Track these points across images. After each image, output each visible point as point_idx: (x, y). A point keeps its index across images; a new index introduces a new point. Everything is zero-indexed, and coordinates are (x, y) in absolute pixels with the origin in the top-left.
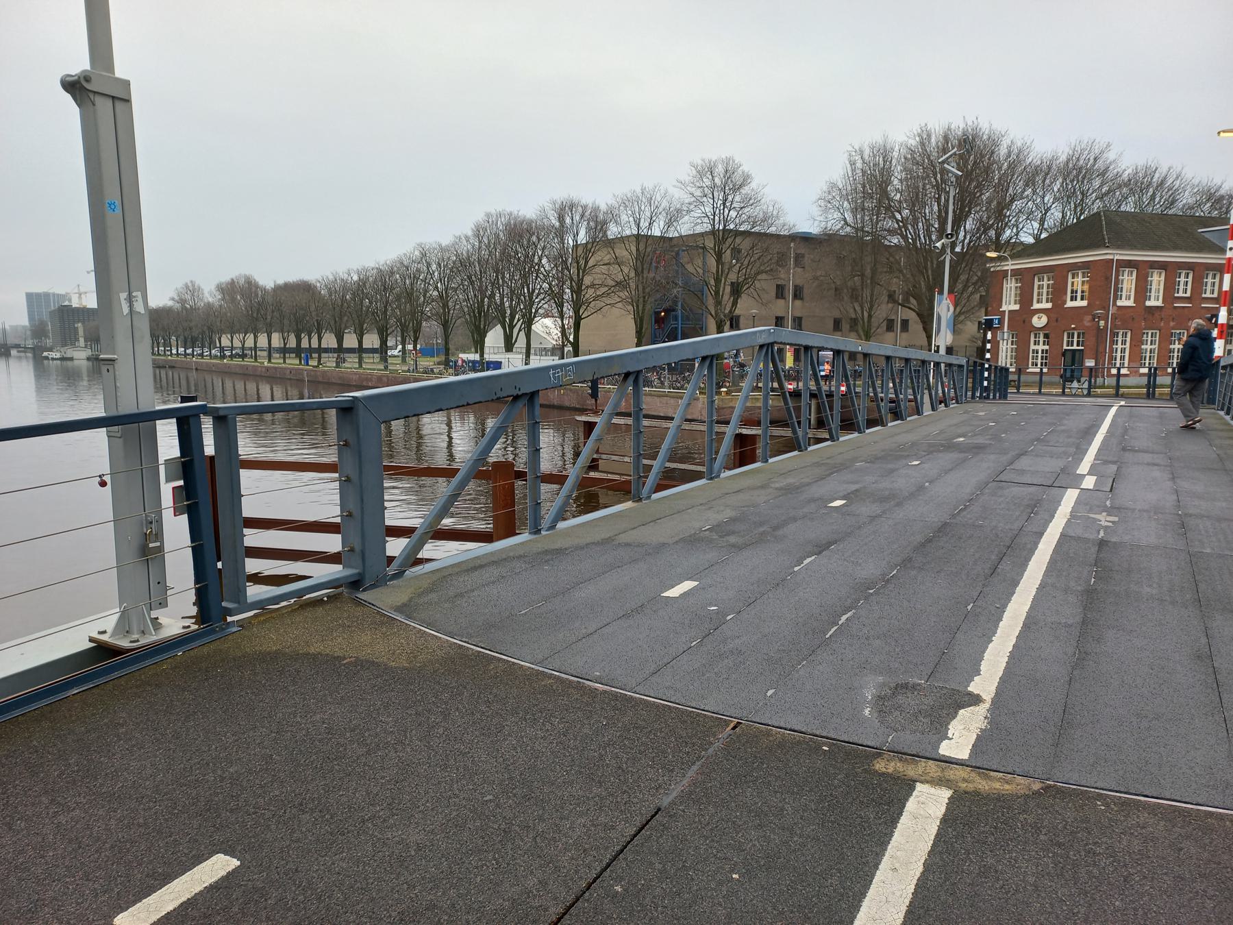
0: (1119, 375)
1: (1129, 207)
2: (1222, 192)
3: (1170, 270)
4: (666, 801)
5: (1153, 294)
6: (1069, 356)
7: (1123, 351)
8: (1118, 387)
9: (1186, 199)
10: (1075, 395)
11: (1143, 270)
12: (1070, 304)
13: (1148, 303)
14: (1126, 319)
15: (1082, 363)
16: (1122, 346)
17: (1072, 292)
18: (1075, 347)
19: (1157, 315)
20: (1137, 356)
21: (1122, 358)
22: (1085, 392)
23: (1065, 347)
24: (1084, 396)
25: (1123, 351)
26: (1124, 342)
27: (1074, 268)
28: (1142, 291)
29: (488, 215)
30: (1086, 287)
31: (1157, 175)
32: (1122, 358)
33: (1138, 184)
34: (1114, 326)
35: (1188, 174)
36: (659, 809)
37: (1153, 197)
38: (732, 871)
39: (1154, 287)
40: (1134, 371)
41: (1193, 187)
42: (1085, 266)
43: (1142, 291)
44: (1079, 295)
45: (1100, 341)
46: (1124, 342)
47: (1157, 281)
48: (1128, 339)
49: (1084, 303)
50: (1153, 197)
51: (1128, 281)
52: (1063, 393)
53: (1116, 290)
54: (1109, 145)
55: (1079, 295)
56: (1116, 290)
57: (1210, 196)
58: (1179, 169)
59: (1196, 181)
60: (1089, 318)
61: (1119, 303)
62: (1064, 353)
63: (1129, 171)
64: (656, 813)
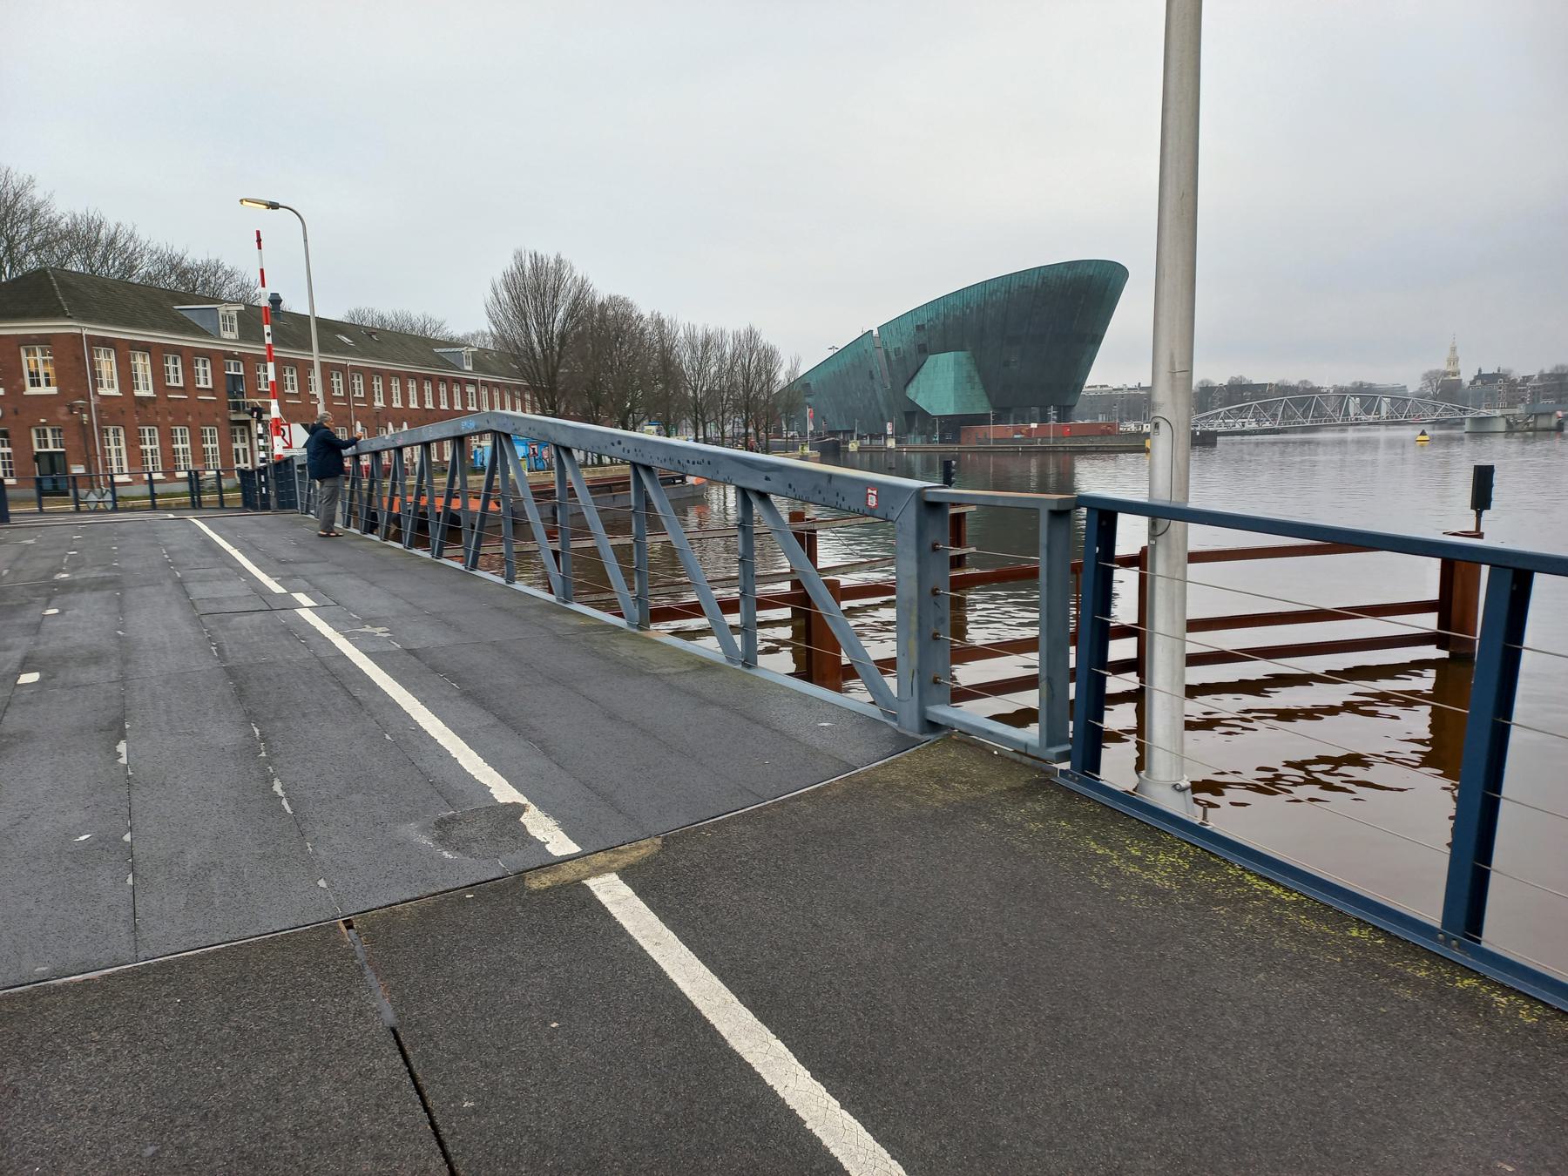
0: (151, 482)
1: (76, 265)
2: (185, 264)
3: (157, 353)
4: (389, 1017)
5: (141, 382)
6: (45, 461)
7: (119, 452)
8: (153, 496)
9: (144, 267)
10: (95, 511)
11: (125, 351)
12: (31, 391)
13: (137, 393)
14: (113, 412)
15: (67, 470)
16: (116, 447)
17: (31, 374)
18: (51, 449)
19: (150, 406)
20: (137, 458)
21: (120, 462)
22: (110, 506)
23: (37, 449)
24: (106, 511)
25: (119, 452)
26: (118, 442)
27: (29, 341)
28: (127, 377)
29: (752, 335)
30: (50, 369)
31: (103, 232)
32: (120, 462)
33: (83, 238)
34: (101, 422)
35: (143, 235)
36: (394, 1030)
37: (105, 258)
38: (546, 1024)
39: (140, 372)
40: (170, 472)
41: (152, 253)
42: (44, 340)
43: (127, 377)
44: (42, 379)
45: (85, 440)
46: (118, 442)
47: (142, 365)
48: (122, 438)
49: (53, 390)
50: (105, 258)
51: (107, 365)
52: (78, 510)
53: (94, 374)
54: (31, 180)
55: (42, 379)
56: (94, 374)
57: (173, 268)
58: (130, 228)
59: (153, 246)
60: (64, 410)
61: (101, 392)
62: (38, 457)
63: (66, 219)
64: (397, 1037)
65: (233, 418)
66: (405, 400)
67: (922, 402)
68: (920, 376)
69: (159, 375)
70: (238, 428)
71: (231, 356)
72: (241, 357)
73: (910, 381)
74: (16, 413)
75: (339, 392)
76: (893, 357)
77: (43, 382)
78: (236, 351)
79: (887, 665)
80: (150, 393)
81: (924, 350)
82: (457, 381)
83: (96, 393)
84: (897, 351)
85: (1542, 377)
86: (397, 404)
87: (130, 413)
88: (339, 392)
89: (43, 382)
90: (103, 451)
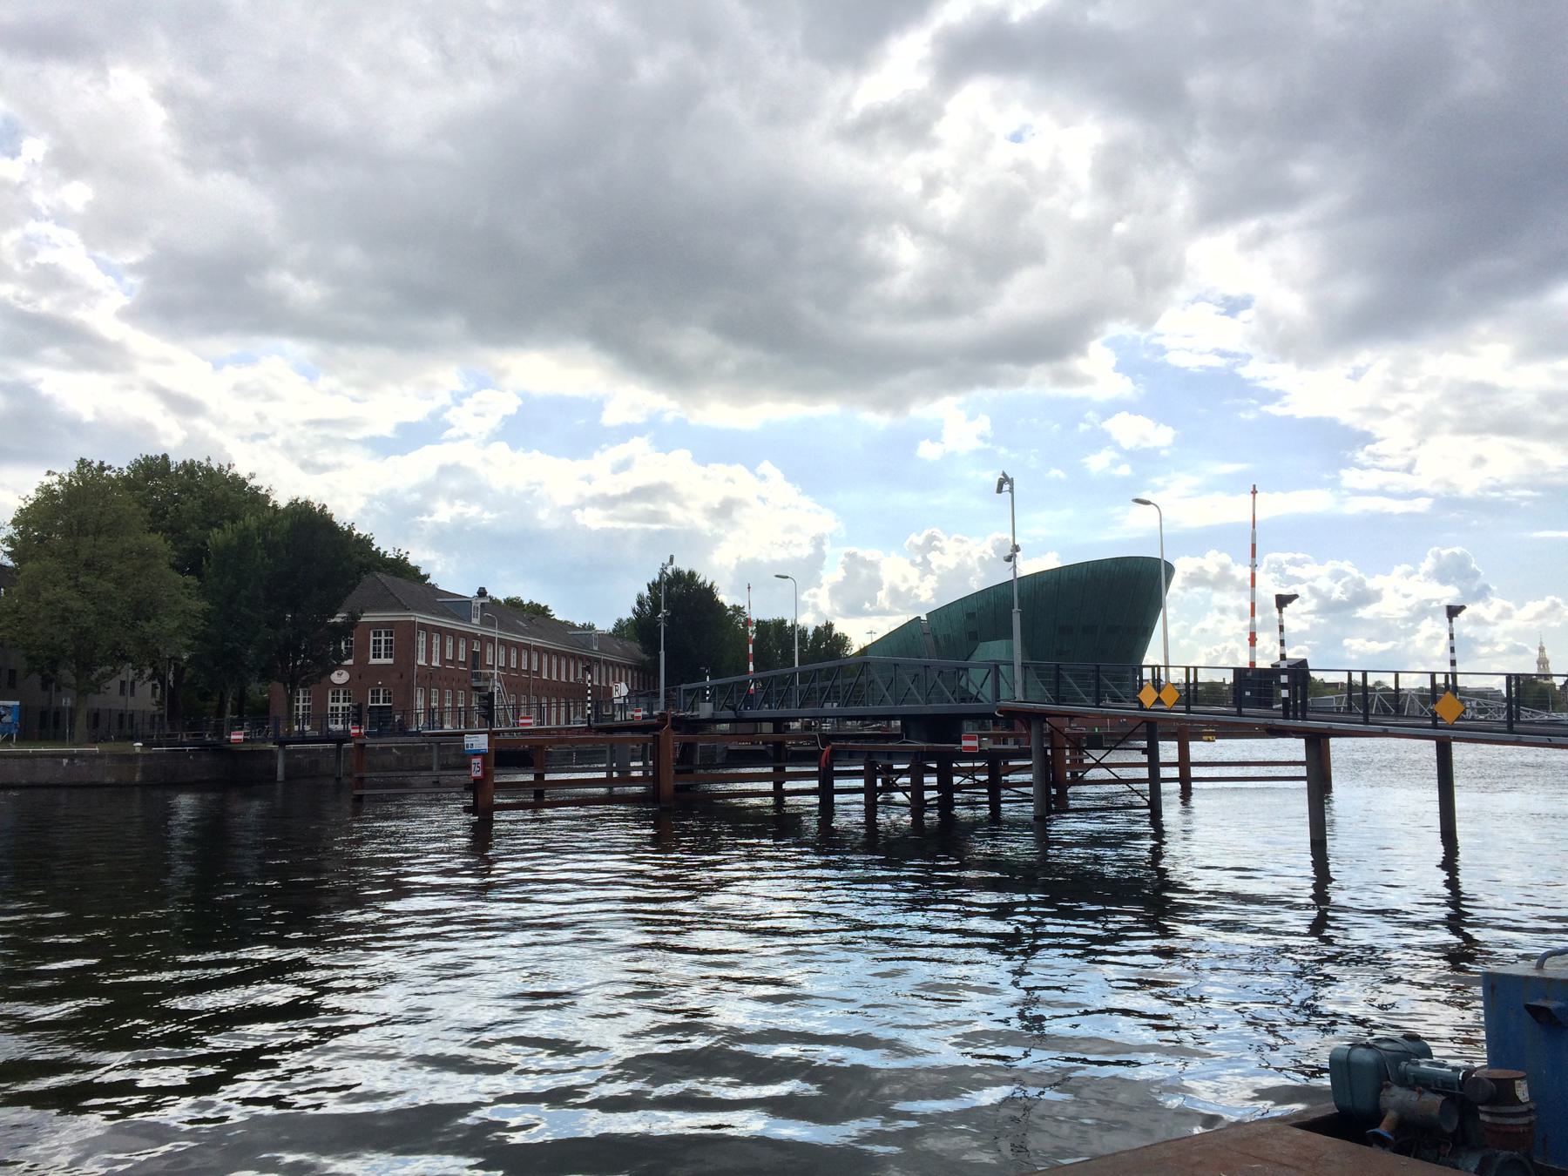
12: (373, 661)
49: (390, 661)
65: (475, 684)
71: (475, 636)
76: (942, 642)
81: (974, 638)
87: (430, 677)
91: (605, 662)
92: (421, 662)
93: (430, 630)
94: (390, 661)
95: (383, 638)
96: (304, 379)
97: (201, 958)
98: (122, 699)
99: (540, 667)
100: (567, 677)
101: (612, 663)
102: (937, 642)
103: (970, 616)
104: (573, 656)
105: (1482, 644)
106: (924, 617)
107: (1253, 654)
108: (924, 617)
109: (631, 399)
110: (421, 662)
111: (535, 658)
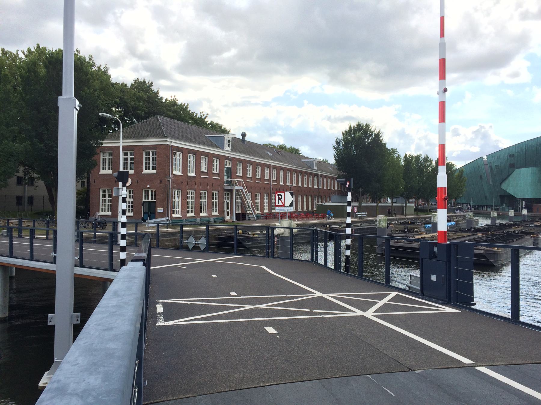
3: (198, 155)
6: (147, 205)
12: (145, 172)
13: (189, 174)
18: (150, 200)
23: (144, 200)
49: (154, 172)
65: (226, 188)
66: (291, 182)
67: (511, 191)
68: (510, 179)
69: (198, 165)
70: (227, 193)
71: (227, 158)
72: (231, 159)
73: (504, 180)
74: (138, 182)
75: (204, 169)
76: (494, 169)
77: (151, 168)
78: (230, 156)
79: (21, 222)
80: (194, 175)
81: (513, 166)
82: (311, 174)
83: (172, 173)
84: (497, 167)
85: (241, 144)
86: (288, 184)
87: (184, 183)
88: (204, 169)
89: (151, 168)
90: (172, 201)
91: (321, 176)
92: (177, 172)
93: (185, 152)
94: (154, 172)
95: (151, 156)
96: (458, 137)
97: (185, 397)
98: (20, 188)
99: (278, 178)
100: (297, 183)
101: (325, 177)
102: (491, 168)
103: (511, 156)
104: (301, 172)
105: (140, 110)
106: (485, 157)
107: (442, 134)
108: (485, 157)
109: (333, 90)
110: (177, 172)
111: (274, 173)
